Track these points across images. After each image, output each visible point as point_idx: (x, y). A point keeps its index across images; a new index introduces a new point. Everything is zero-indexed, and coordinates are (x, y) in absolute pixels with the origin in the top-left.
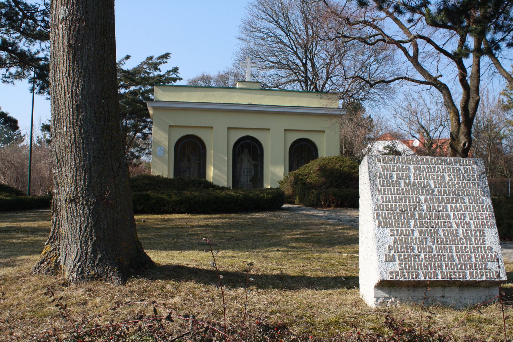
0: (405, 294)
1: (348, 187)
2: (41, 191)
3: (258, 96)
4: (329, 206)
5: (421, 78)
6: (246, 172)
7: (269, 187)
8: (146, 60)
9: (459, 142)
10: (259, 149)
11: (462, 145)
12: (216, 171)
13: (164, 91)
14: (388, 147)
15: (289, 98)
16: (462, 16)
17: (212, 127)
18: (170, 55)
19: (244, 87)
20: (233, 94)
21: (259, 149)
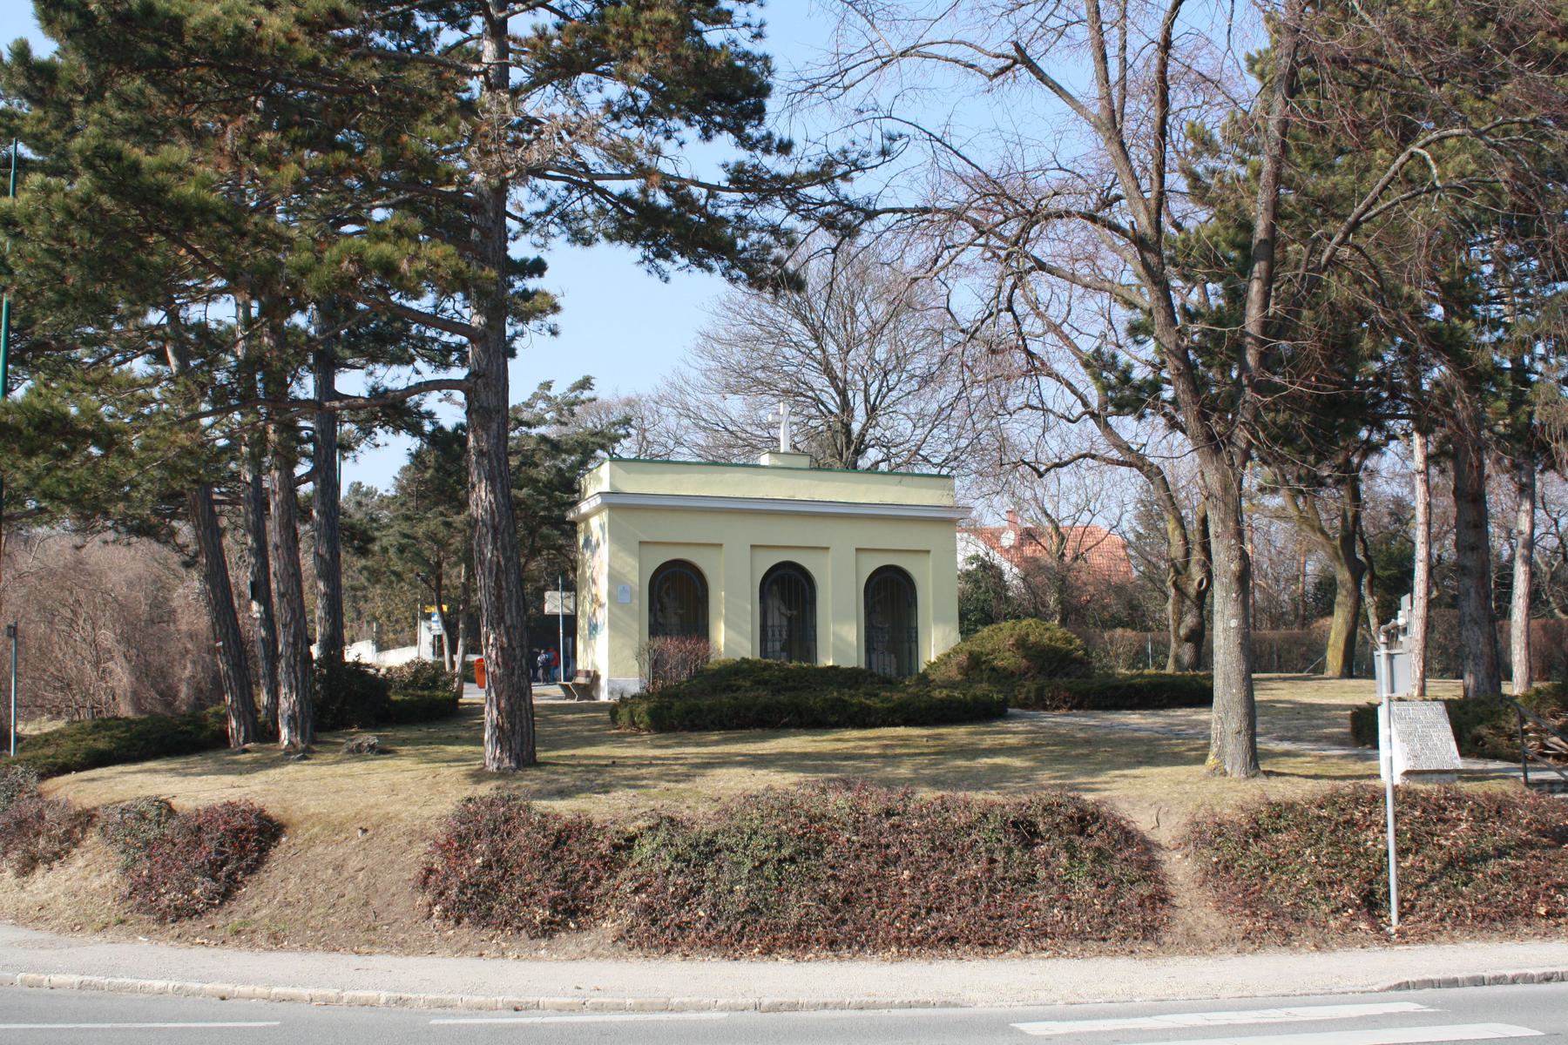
0: (1414, 777)
1: (1067, 675)
2: (189, 665)
3: (807, 481)
4: (1058, 708)
5: (1115, 454)
6: (777, 633)
7: (830, 663)
8: (539, 388)
9: (1189, 577)
10: (807, 587)
11: (1196, 583)
12: (731, 633)
13: (629, 473)
14: (976, 558)
15: (863, 487)
16: (1512, 698)
17: (721, 545)
18: (593, 381)
19: (780, 464)
20: (761, 478)
21: (807, 587)
